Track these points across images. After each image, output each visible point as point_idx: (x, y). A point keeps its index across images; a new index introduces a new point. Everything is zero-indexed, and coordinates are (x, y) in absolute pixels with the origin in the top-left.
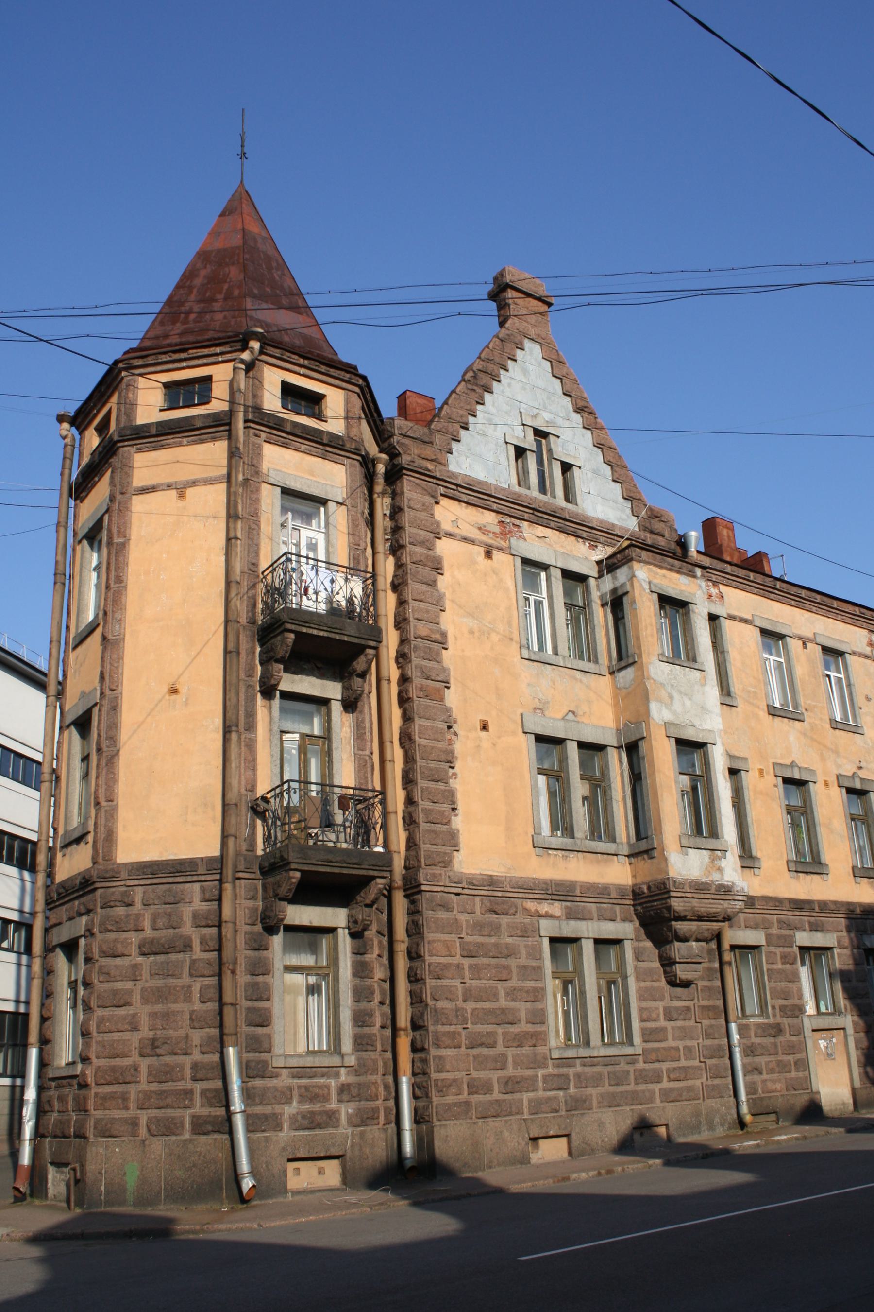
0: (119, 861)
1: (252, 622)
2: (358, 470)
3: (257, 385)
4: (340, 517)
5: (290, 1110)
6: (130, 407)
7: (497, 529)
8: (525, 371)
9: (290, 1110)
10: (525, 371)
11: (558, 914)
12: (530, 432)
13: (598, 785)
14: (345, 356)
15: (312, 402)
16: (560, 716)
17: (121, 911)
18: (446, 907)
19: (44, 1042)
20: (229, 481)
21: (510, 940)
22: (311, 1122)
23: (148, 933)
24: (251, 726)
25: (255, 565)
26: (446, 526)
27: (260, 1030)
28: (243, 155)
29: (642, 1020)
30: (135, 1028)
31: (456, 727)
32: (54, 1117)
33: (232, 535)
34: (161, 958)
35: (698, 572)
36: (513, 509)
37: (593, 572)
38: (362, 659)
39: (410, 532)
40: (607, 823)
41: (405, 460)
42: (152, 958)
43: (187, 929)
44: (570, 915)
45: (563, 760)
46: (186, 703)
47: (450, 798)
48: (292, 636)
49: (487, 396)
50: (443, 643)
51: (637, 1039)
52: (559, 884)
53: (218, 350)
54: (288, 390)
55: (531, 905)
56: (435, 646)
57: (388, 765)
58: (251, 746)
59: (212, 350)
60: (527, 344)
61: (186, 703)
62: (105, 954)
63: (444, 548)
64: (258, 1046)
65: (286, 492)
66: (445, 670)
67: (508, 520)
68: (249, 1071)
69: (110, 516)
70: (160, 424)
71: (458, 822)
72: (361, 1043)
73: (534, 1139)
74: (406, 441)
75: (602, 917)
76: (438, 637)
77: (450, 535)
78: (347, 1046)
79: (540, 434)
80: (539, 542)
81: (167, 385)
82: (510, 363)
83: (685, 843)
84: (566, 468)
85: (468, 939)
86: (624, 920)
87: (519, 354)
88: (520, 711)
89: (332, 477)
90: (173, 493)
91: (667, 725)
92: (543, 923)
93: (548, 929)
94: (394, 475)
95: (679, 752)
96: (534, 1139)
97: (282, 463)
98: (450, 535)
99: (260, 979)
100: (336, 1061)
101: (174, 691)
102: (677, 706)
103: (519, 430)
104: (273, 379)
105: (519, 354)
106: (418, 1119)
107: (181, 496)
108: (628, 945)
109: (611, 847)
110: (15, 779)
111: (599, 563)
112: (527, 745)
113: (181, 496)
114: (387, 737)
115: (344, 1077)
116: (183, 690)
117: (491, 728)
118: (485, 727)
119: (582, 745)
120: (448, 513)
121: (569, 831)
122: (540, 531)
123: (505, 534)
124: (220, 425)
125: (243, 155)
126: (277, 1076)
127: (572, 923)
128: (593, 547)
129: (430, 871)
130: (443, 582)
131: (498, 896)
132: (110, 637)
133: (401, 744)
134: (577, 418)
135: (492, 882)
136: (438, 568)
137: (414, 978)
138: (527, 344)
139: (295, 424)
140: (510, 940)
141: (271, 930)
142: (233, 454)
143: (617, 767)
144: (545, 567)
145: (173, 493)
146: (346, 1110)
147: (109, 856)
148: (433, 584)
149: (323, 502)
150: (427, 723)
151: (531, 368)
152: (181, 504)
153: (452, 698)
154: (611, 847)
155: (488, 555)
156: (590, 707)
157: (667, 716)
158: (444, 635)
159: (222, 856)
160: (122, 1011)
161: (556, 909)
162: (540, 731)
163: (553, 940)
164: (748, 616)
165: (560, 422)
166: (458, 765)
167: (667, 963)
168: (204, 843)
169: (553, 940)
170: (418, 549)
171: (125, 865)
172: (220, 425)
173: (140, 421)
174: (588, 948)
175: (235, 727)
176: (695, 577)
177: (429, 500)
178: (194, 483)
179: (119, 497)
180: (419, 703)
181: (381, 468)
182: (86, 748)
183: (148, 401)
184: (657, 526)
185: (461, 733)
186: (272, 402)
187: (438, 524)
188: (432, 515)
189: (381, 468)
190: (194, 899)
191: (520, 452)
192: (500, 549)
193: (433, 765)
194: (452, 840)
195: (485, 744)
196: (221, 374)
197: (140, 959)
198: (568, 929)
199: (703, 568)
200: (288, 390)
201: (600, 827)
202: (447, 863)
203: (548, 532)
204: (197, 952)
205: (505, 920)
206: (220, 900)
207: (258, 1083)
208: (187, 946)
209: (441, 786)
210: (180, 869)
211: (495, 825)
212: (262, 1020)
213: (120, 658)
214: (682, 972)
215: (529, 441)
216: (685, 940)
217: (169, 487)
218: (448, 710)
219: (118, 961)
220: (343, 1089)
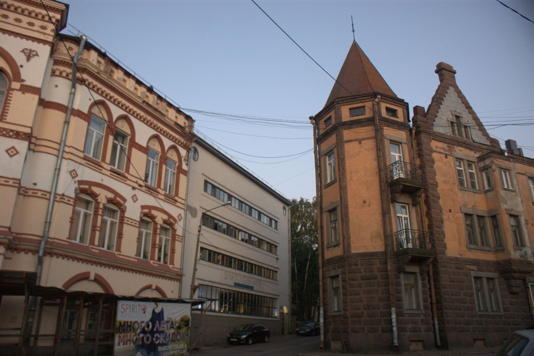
0: (353, 251)
1: (387, 181)
2: (409, 133)
3: (379, 109)
4: (405, 147)
5: (409, 326)
6: (339, 115)
7: (447, 148)
8: (450, 96)
9: (409, 326)
10: (450, 96)
11: (475, 269)
12: (454, 117)
13: (482, 228)
14: (400, 96)
15: (393, 112)
16: (470, 207)
17: (354, 267)
18: (444, 266)
19: (325, 305)
20: (376, 138)
21: (462, 277)
22: (415, 330)
23: (364, 274)
24: (389, 213)
25: (386, 164)
26: (434, 149)
27: (399, 302)
28: (353, 31)
29: (503, 304)
30: (362, 301)
31: (443, 212)
32: (331, 327)
33: (379, 155)
34: (368, 281)
35: (512, 160)
36: (452, 142)
37: (476, 160)
38: (420, 192)
39: (425, 151)
40: (486, 241)
41: (421, 129)
42: (365, 281)
43: (376, 272)
44: (479, 270)
45: (472, 221)
46: (369, 206)
47: (443, 233)
48: (402, 186)
49: (441, 106)
50: (437, 186)
51: (502, 311)
52: (475, 260)
53: (366, 98)
54: (388, 109)
55: (468, 266)
56: (435, 186)
57: (424, 223)
58: (390, 218)
59: (364, 98)
60: (450, 88)
61: (369, 206)
62: (350, 280)
63: (435, 155)
64: (399, 307)
65: (391, 140)
66: (438, 194)
67: (450, 145)
68: (398, 315)
69: (337, 150)
70: (351, 121)
71: (446, 240)
72: (425, 307)
73: (475, 340)
74: (420, 122)
75: (488, 271)
76: (435, 183)
77: (435, 151)
78: (422, 308)
79: (457, 117)
80: (461, 152)
81: (350, 109)
82: (446, 94)
83: (515, 248)
84: (466, 127)
85: (451, 276)
86: (495, 272)
87: (448, 91)
88: (459, 206)
89: (402, 135)
90: (357, 142)
91: (506, 209)
92: (472, 272)
93: (473, 274)
94: (418, 133)
95: (465, 217)
96: (475, 340)
97: (389, 132)
98: (435, 151)
99: (398, 287)
100: (417, 312)
101: (365, 202)
102: (509, 203)
103: (451, 117)
104: (383, 106)
105: (448, 91)
106: (441, 331)
107: (360, 143)
108: (496, 280)
109: (489, 249)
110: (208, 227)
111: (478, 158)
112: (461, 216)
113: (360, 143)
114: (423, 215)
115: (422, 317)
116: (368, 202)
117: (452, 211)
118: (450, 211)
119: (478, 216)
120: (434, 144)
121: (476, 243)
122: (460, 148)
123: (450, 150)
124: (370, 121)
125: (353, 31)
126: (404, 316)
127: (480, 272)
128: (475, 153)
129: (440, 255)
130: (435, 166)
131: (459, 263)
132: (342, 186)
133: (427, 217)
134: (466, 110)
135: (457, 259)
136: (433, 162)
137: (436, 287)
138: (450, 88)
139: (392, 120)
140: (462, 277)
141: (400, 272)
142: (376, 131)
143: (488, 223)
144: (462, 160)
145: (357, 142)
146: (423, 327)
147: (349, 251)
148: (432, 167)
149: (401, 143)
150: (435, 210)
151: (452, 95)
152: (360, 146)
153: (441, 202)
154: (489, 249)
155: (446, 157)
156: (479, 204)
157: (506, 207)
158: (437, 183)
159: (386, 250)
160: (357, 297)
161: (475, 268)
162: (466, 212)
163: (474, 277)
164: (524, 173)
165: (462, 112)
166: (444, 222)
167: (509, 286)
168: (378, 246)
169: (474, 277)
170: (427, 156)
171: (355, 254)
172: (370, 121)
173: (344, 120)
174: (485, 280)
175: (385, 213)
176: (510, 161)
177: (428, 140)
178: (364, 139)
179: (340, 144)
180: (432, 204)
181: (414, 131)
182: (494, 222)
183: (345, 114)
184: (495, 145)
185: (444, 213)
186: (384, 114)
187: (432, 148)
188: (430, 145)
189: (414, 131)
190: (377, 264)
191: (452, 123)
192: (449, 155)
193: (438, 223)
194: (445, 246)
195: (451, 217)
196: (368, 105)
197: (361, 281)
198: (480, 274)
199: (513, 158)
200: (388, 109)
201: (485, 242)
202: (444, 253)
203: (462, 149)
204: (379, 279)
205: (461, 271)
206: (386, 263)
207: (400, 318)
208: (376, 278)
209: (440, 229)
210: (372, 255)
211: (454, 242)
212: (400, 300)
213: (347, 192)
214: (515, 290)
215: (454, 120)
216: (515, 279)
217: (356, 140)
218: (440, 206)
219: (355, 282)
220: (422, 321)
